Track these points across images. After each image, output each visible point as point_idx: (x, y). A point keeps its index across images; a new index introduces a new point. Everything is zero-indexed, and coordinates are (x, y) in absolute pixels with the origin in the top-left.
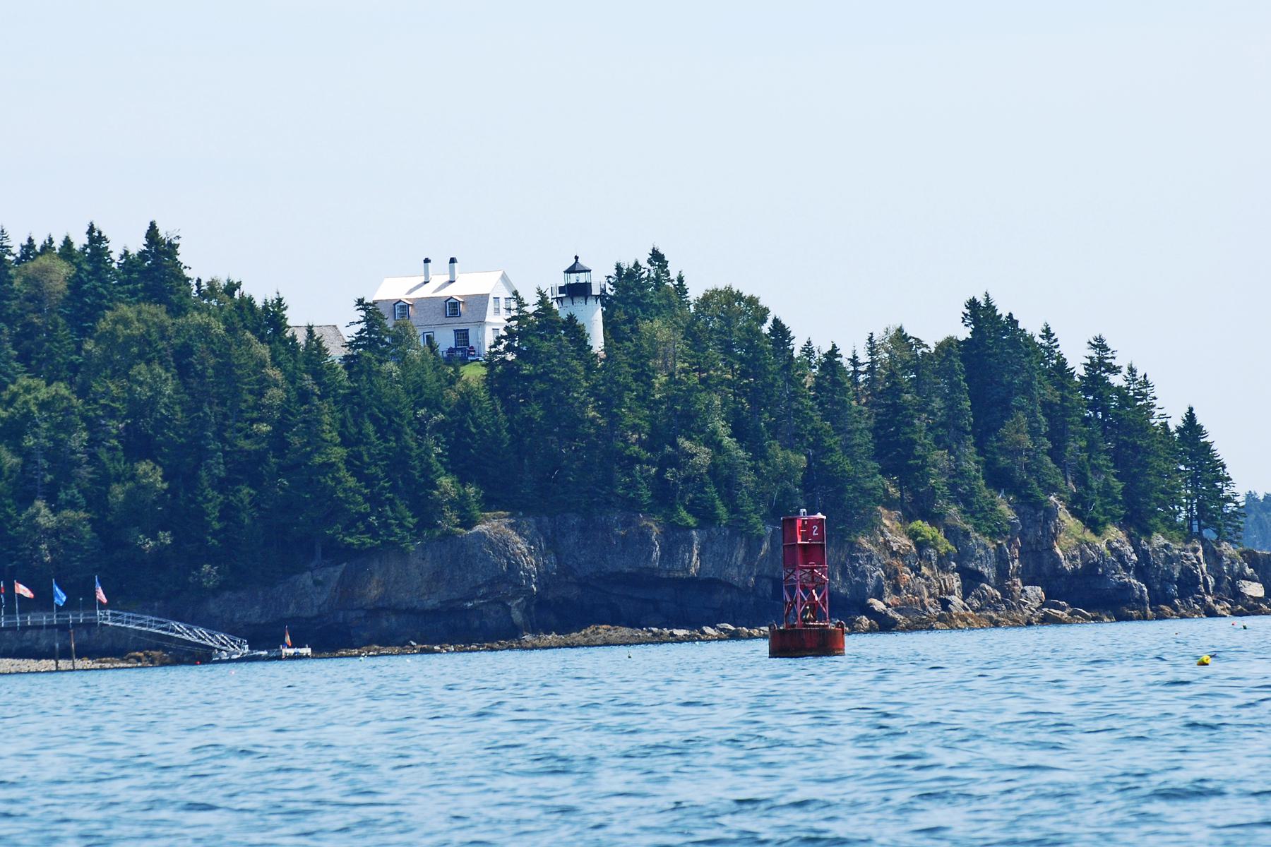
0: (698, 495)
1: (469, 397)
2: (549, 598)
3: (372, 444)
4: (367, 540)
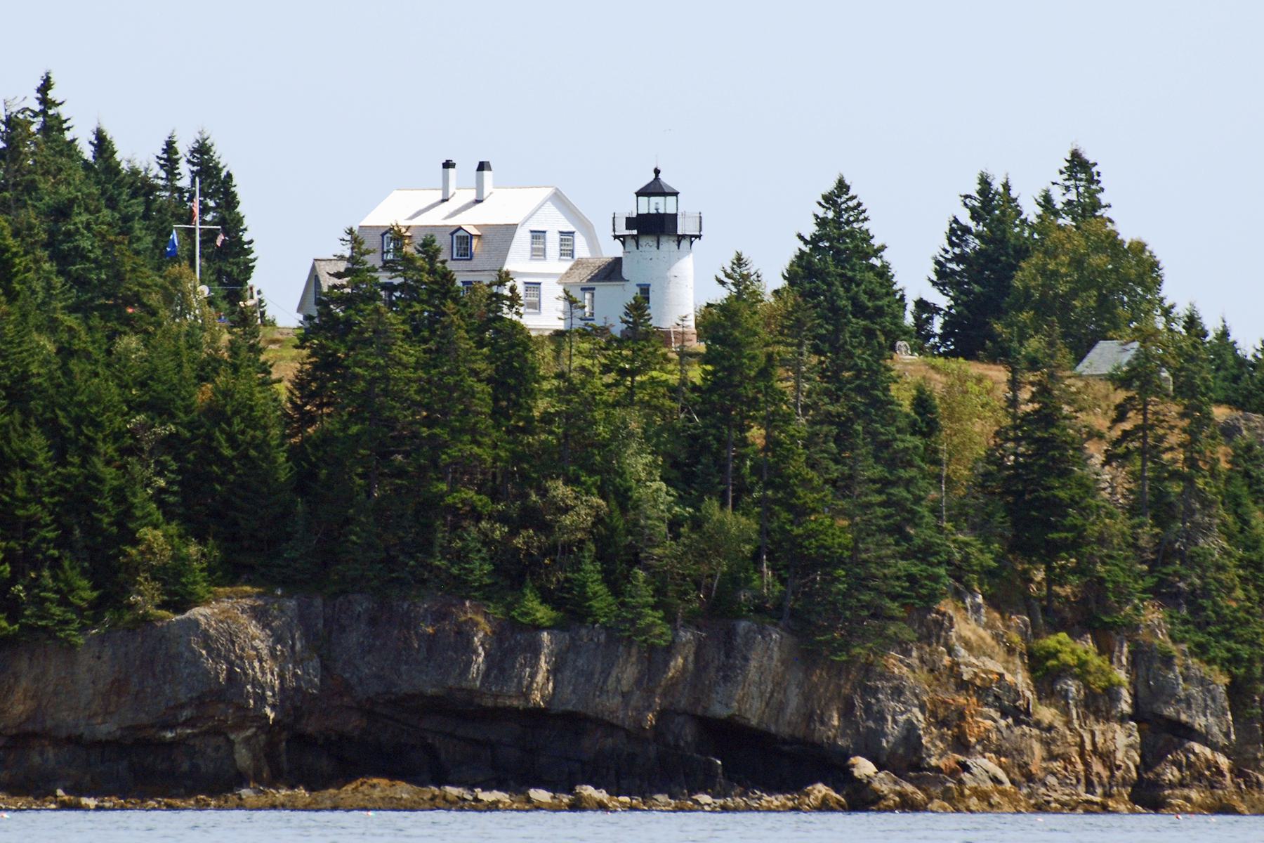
2: (310, 729)
3: (37, 468)
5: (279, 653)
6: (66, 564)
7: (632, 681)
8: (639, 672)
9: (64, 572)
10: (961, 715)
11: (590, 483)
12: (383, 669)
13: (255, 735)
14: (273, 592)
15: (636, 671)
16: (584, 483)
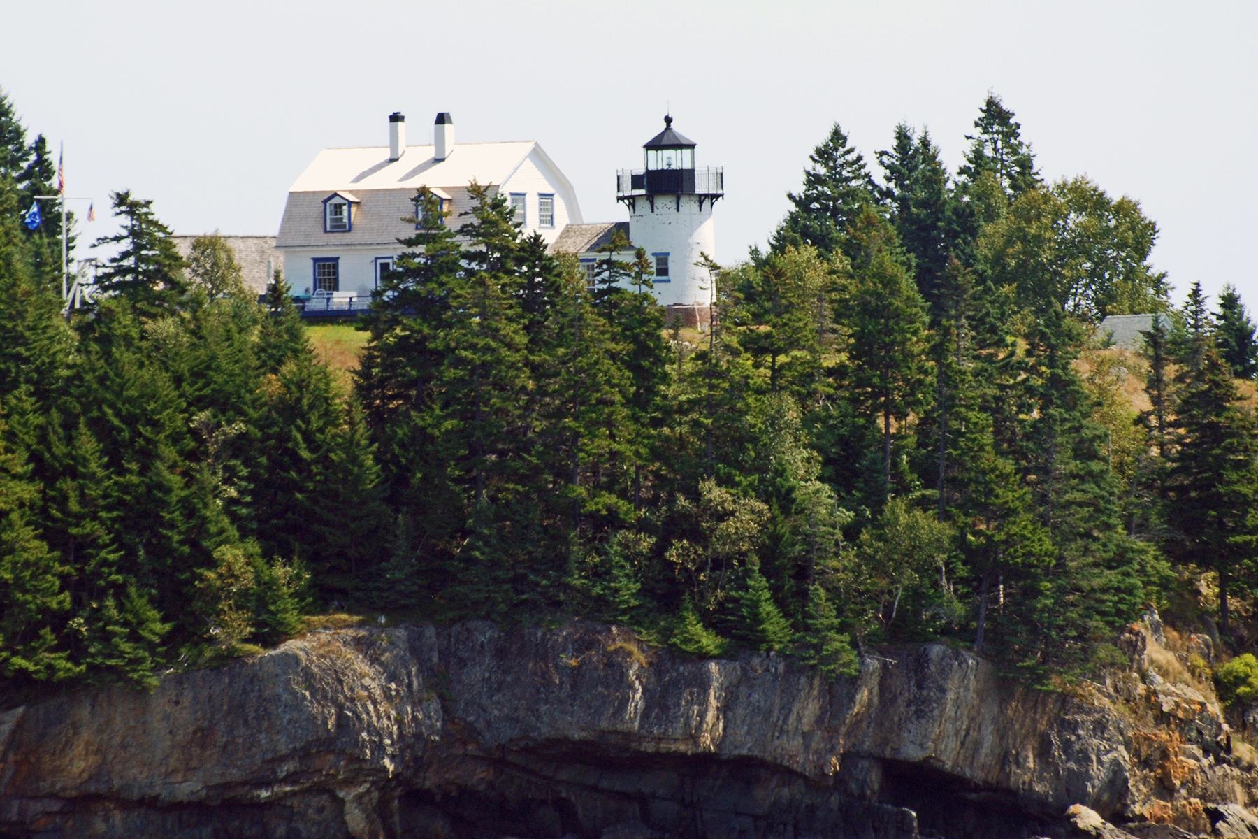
0: (733, 593)
1: (300, 387)
2: (428, 784)
3: (92, 476)
4: (62, 663)
5: (394, 693)
6: (132, 590)
7: (813, 719)
8: (820, 708)
9: (132, 602)
10: (1165, 755)
11: (745, 483)
12: (516, 709)
13: (368, 791)
14: (375, 619)
15: (817, 707)
16: (738, 484)
